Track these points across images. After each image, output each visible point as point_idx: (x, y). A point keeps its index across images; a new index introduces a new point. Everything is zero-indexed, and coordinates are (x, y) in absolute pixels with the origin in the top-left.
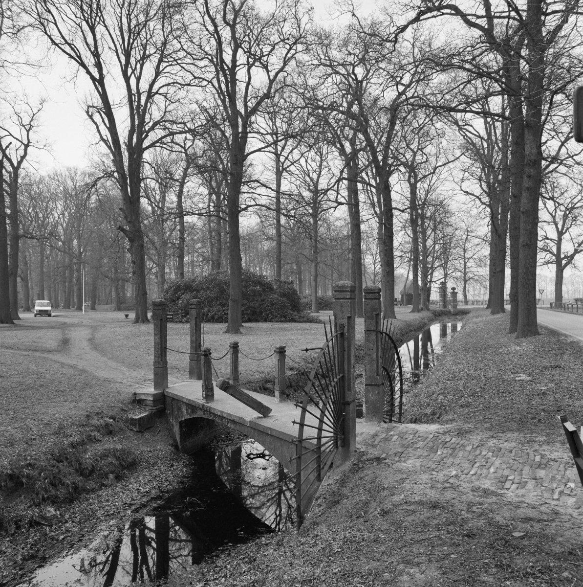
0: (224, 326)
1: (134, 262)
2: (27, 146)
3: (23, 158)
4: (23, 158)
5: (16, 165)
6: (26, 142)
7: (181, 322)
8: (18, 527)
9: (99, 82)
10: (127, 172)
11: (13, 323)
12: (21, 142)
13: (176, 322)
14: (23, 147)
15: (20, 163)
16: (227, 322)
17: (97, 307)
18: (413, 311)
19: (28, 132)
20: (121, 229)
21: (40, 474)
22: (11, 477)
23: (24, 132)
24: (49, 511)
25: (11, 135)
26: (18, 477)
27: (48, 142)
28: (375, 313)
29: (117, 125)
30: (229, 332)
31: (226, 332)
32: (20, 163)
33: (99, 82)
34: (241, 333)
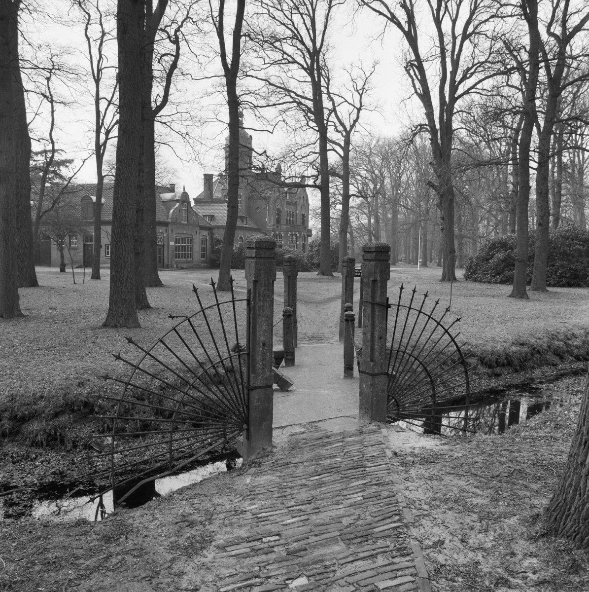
0: (508, 289)
1: (443, 219)
2: (359, 110)
3: (355, 121)
4: (355, 121)
5: (348, 129)
6: (358, 106)
7: (489, 282)
8: (75, 447)
9: (412, 39)
10: (438, 126)
11: (332, 275)
12: (353, 106)
13: (484, 282)
14: (356, 111)
15: (352, 126)
16: (512, 283)
17: (428, 263)
18: (318, 275)
19: (361, 96)
20: (430, 184)
21: (113, 407)
22: (86, 404)
23: (357, 96)
24: (108, 440)
25: (346, 101)
26: (93, 406)
27: (379, 103)
28: (371, 279)
29: (427, 78)
30: (513, 297)
31: (510, 296)
32: (352, 126)
33: (412, 39)
34: (528, 298)
